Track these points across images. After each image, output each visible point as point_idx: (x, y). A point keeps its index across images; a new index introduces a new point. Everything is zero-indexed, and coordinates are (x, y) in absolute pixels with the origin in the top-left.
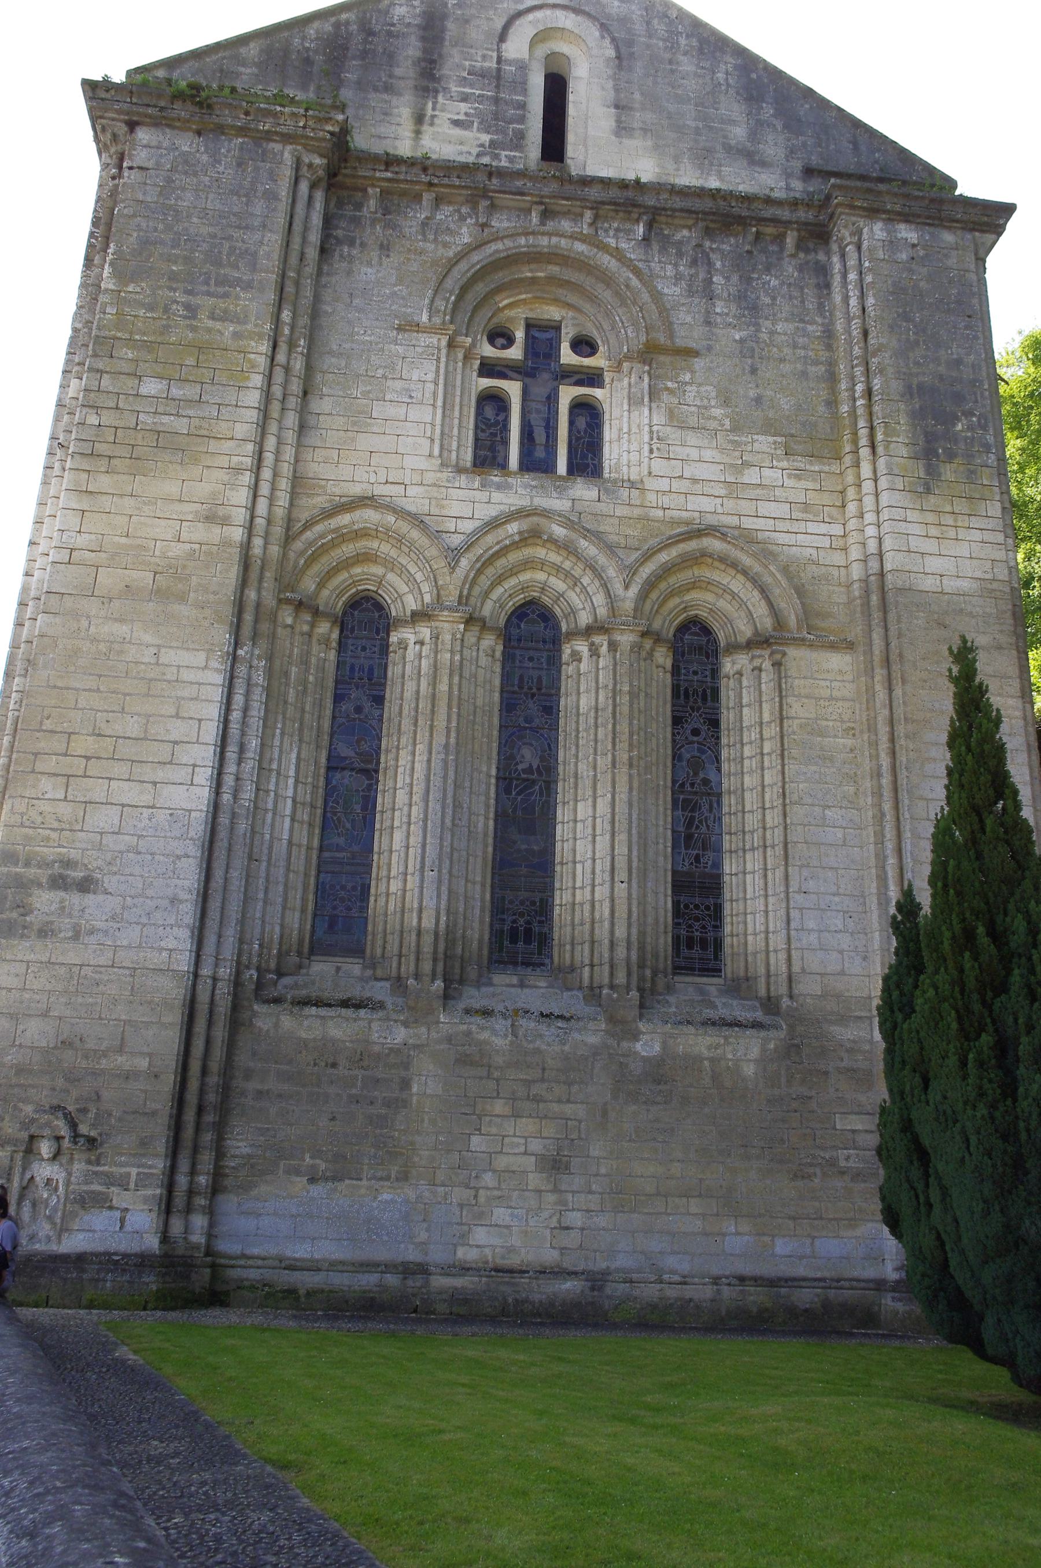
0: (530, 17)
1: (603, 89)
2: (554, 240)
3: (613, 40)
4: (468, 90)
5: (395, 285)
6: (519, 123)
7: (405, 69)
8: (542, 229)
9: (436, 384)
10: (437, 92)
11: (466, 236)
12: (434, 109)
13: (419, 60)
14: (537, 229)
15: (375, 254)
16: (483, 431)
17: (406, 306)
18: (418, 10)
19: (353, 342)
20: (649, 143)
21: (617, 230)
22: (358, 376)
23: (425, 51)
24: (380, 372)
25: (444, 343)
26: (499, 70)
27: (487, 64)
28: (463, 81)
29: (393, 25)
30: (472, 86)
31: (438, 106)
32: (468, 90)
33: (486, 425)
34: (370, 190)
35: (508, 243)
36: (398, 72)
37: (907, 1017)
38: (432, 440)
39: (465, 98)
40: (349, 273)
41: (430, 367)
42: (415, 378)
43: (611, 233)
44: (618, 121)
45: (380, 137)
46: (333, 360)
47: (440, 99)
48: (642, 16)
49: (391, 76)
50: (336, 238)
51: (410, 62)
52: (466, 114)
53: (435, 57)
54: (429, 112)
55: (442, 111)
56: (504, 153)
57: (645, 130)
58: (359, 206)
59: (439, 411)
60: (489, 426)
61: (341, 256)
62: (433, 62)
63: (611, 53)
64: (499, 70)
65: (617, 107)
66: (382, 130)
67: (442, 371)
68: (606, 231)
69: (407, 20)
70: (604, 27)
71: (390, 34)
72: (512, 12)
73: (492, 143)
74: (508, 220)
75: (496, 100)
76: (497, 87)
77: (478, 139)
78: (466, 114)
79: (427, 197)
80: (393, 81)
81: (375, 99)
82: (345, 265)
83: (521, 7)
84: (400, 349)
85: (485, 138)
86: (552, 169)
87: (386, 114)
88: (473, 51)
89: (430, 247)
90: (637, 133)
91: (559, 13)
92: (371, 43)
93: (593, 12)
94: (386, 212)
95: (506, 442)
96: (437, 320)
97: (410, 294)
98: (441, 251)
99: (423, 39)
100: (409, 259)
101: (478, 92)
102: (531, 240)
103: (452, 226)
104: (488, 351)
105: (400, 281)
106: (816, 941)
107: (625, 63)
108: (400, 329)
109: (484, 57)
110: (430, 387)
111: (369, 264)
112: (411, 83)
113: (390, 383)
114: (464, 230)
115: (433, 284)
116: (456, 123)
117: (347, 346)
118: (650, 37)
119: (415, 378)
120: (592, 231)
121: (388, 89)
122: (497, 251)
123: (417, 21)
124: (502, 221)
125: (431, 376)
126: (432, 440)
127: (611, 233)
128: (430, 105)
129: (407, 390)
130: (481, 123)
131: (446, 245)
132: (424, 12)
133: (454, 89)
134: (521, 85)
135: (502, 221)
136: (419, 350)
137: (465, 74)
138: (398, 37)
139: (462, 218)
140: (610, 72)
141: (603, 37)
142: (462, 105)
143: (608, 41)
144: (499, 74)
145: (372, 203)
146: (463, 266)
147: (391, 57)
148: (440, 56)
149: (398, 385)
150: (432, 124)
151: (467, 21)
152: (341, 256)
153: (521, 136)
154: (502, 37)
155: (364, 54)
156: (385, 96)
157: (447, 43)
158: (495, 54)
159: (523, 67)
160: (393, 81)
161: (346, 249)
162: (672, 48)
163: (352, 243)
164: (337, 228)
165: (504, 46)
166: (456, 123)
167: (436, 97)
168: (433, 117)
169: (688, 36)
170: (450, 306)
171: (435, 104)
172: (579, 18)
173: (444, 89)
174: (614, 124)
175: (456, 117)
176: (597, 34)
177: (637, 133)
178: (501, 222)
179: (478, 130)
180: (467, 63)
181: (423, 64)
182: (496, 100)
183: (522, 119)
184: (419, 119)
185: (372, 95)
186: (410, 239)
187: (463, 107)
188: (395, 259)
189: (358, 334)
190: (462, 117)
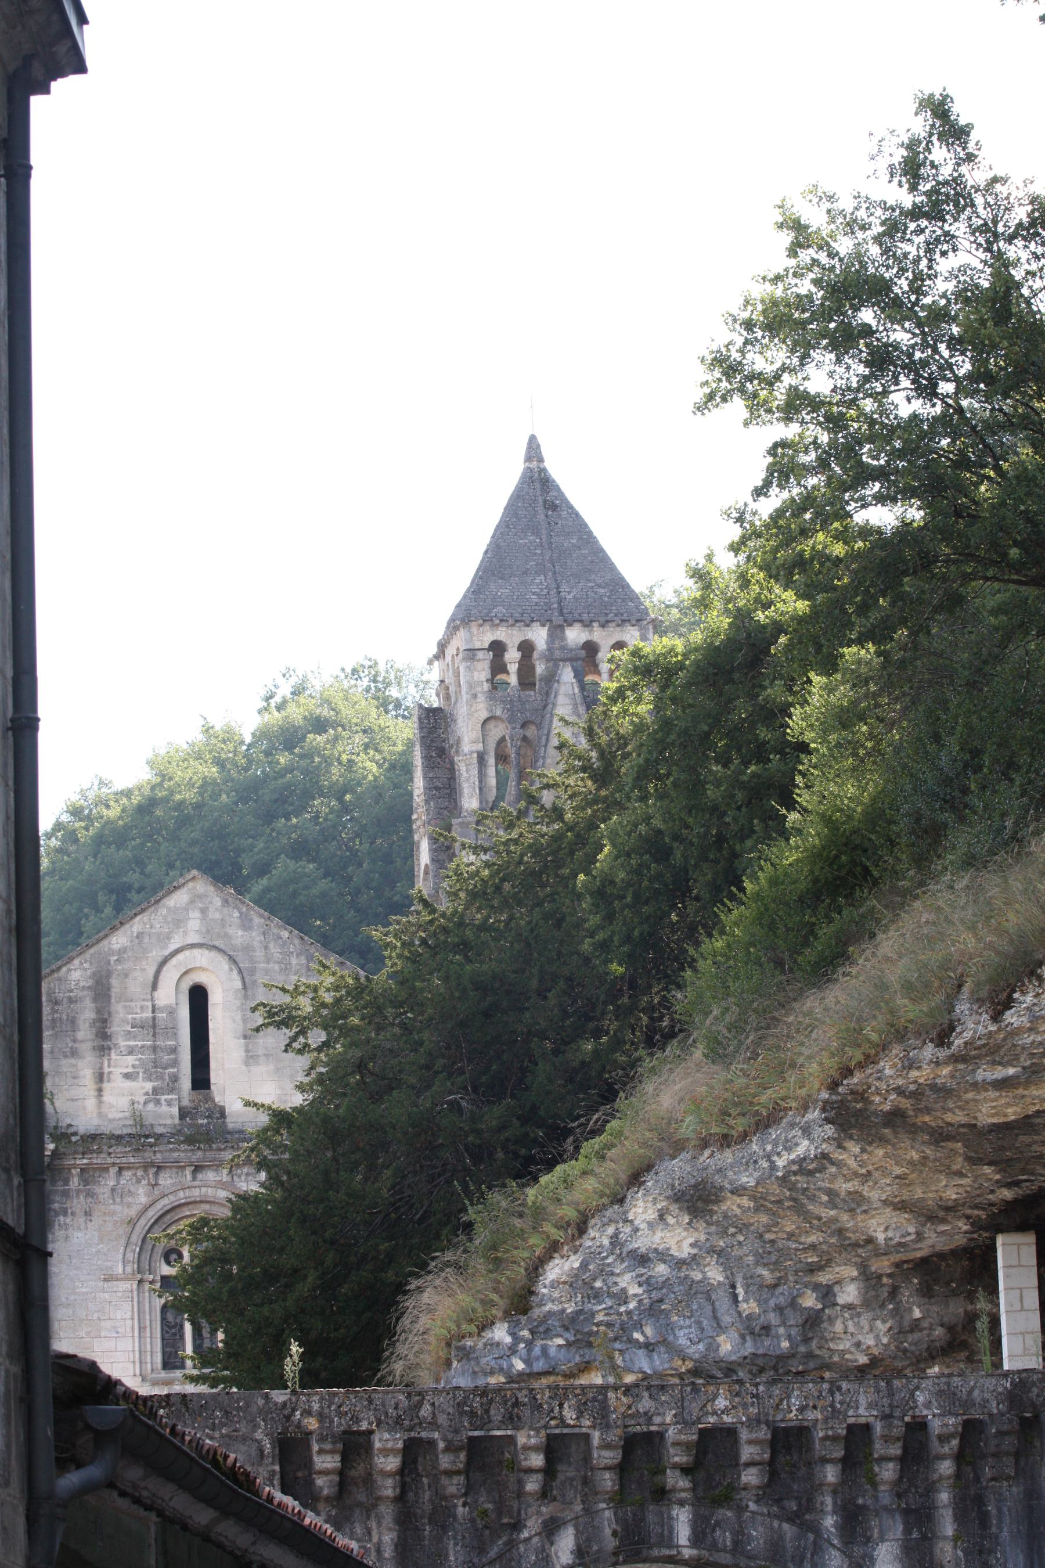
0: (174, 961)
1: (234, 1021)
2: (204, 1190)
3: (240, 971)
4: (132, 1043)
5: (98, 1244)
6: (173, 1067)
7: (85, 1032)
8: (197, 1183)
9: (133, 1319)
10: (110, 1049)
11: (142, 1195)
12: (109, 1066)
13: (94, 1021)
14: (190, 1184)
15: (82, 1220)
16: (167, 1332)
17: (107, 1260)
18: (89, 972)
19: (75, 1294)
20: (271, 1067)
21: (247, 1174)
22: (82, 1320)
23: (98, 1011)
24: (96, 1315)
25: (135, 1286)
26: (154, 1018)
27: (145, 1015)
28: (128, 1035)
29: (71, 991)
30: (135, 1038)
31: (112, 1062)
32: (132, 1043)
33: (169, 1327)
34: (73, 1171)
35: (172, 1198)
36: (80, 1035)
37: (800, 1088)
38: (134, 1362)
39: (131, 1051)
40: (67, 1238)
41: (127, 1307)
42: (119, 1317)
43: (243, 1178)
44: (247, 1051)
45: (72, 1100)
46: (64, 1310)
47: (113, 1056)
48: (261, 942)
49: (75, 1041)
50: (54, 1210)
51: (87, 1025)
52: (133, 1066)
53: (106, 1016)
54: (106, 1070)
55: (116, 1067)
56: (163, 1097)
57: (267, 1056)
58: (66, 1182)
59: (137, 1340)
60: (170, 1328)
61: (59, 1225)
62: (105, 1021)
63: (238, 984)
64: (154, 1018)
65: (245, 1037)
66: (75, 1092)
67: (136, 1309)
68: (239, 1177)
69: (82, 984)
70: (232, 960)
71: (71, 1001)
72: (160, 959)
73: (155, 1091)
74: (170, 1177)
75: (154, 1049)
76: (154, 1035)
77: (143, 1088)
78: (133, 1066)
79: (113, 1171)
80: (76, 1045)
81: (66, 1063)
82: (63, 1232)
83: (167, 952)
84: (106, 1296)
85: (149, 1086)
86: (200, 1094)
87: (75, 1078)
88: (133, 1004)
89: (118, 1208)
90: (262, 1059)
91: (196, 952)
92: (57, 1012)
93: (222, 947)
94: (86, 1183)
95: (182, 1337)
96: (129, 1269)
97: (109, 1250)
98: (126, 1211)
99: (95, 1000)
100: (105, 1221)
101: (140, 1043)
102: (188, 1192)
103: (132, 1189)
104: (167, 1270)
105: (101, 1240)
106: (456, 1480)
107: (249, 992)
108: (105, 1280)
109: (142, 1007)
110: (129, 1322)
111: (79, 1229)
112: (89, 1045)
113: (103, 1323)
114: (141, 1191)
115: (123, 1241)
116: (127, 1076)
117: (72, 1298)
118: (268, 962)
119: (119, 1317)
120: (229, 1179)
121: (74, 1053)
122: (165, 1206)
123: (90, 983)
124: (166, 1179)
125: (129, 1315)
126: (134, 1362)
127: (243, 1178)
128: (106, 1064)
129: (114, 1327)
130: (144, 1072)
131: (129, 1206)
132: (94, 974)
133: (123, 1043)
134: (172, 1030)
135: (166, 1179)
136: (120, 1294)
137: (129, 1029)
138: (76, 1002)
139: (139, 1181)
140: (238, 1003)
141: (231, 970)
142: (130, 1057)
143: (235, 972)
144: (154, 1023)
145: (76, 1179)
146: (142, 1222)
147: (73, 1022)
148: (110, 1014)
149: (107, 1324)
150: (109, 1081)
151: (126, 976)
152: (59, 1225)
153: (175, 1079)
154: (154, 986)
155: (54, 1020)
156: (73, 1061)
157: (113, 1000)
158: (149, 1004)
159: (172, 1012)
160: (76, 1045)
161: (62, 1218)
162: (286, 969)
163: (65, 1214)
164: (54, 1202)
165: (156, 994)
166: (127, 1076)
167: (109, 1055)
168: (110, 1073)
169: (298, 955)
170: (136, 1256)
171: (109, 1060)
172: (213, 954)
173: (115, 1045)
174: (244, 1054)
175: (126, 1071)
176: (226, 967)
177: (262, 1059)
178: (166, 1180)
179: (144, 1079)
180: (130, 1017)
181: (98, 1024)
182: (154, 1049)
183: (175, 1063)
184: (100, 1077)
185: (64, 1062)
186: (104, 1204)
187: (131, 1059)
188: (96, 1221)
189: (78, 1287)
190: (130, 1070)
